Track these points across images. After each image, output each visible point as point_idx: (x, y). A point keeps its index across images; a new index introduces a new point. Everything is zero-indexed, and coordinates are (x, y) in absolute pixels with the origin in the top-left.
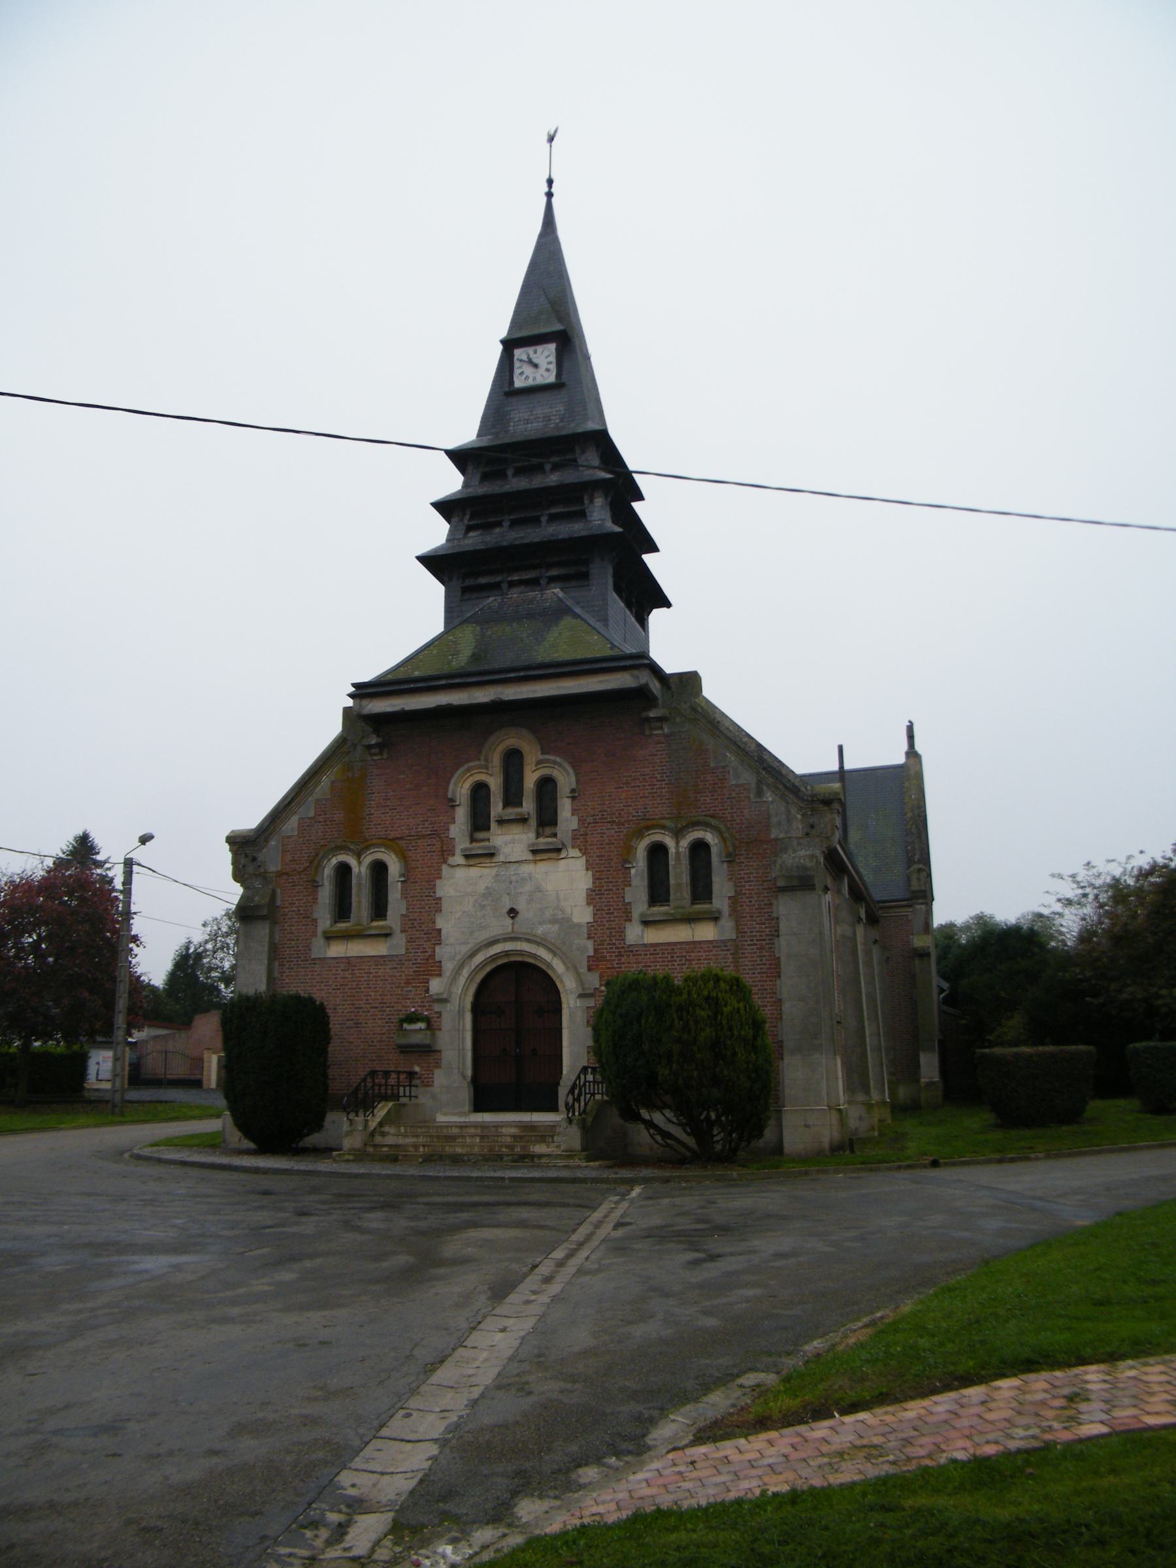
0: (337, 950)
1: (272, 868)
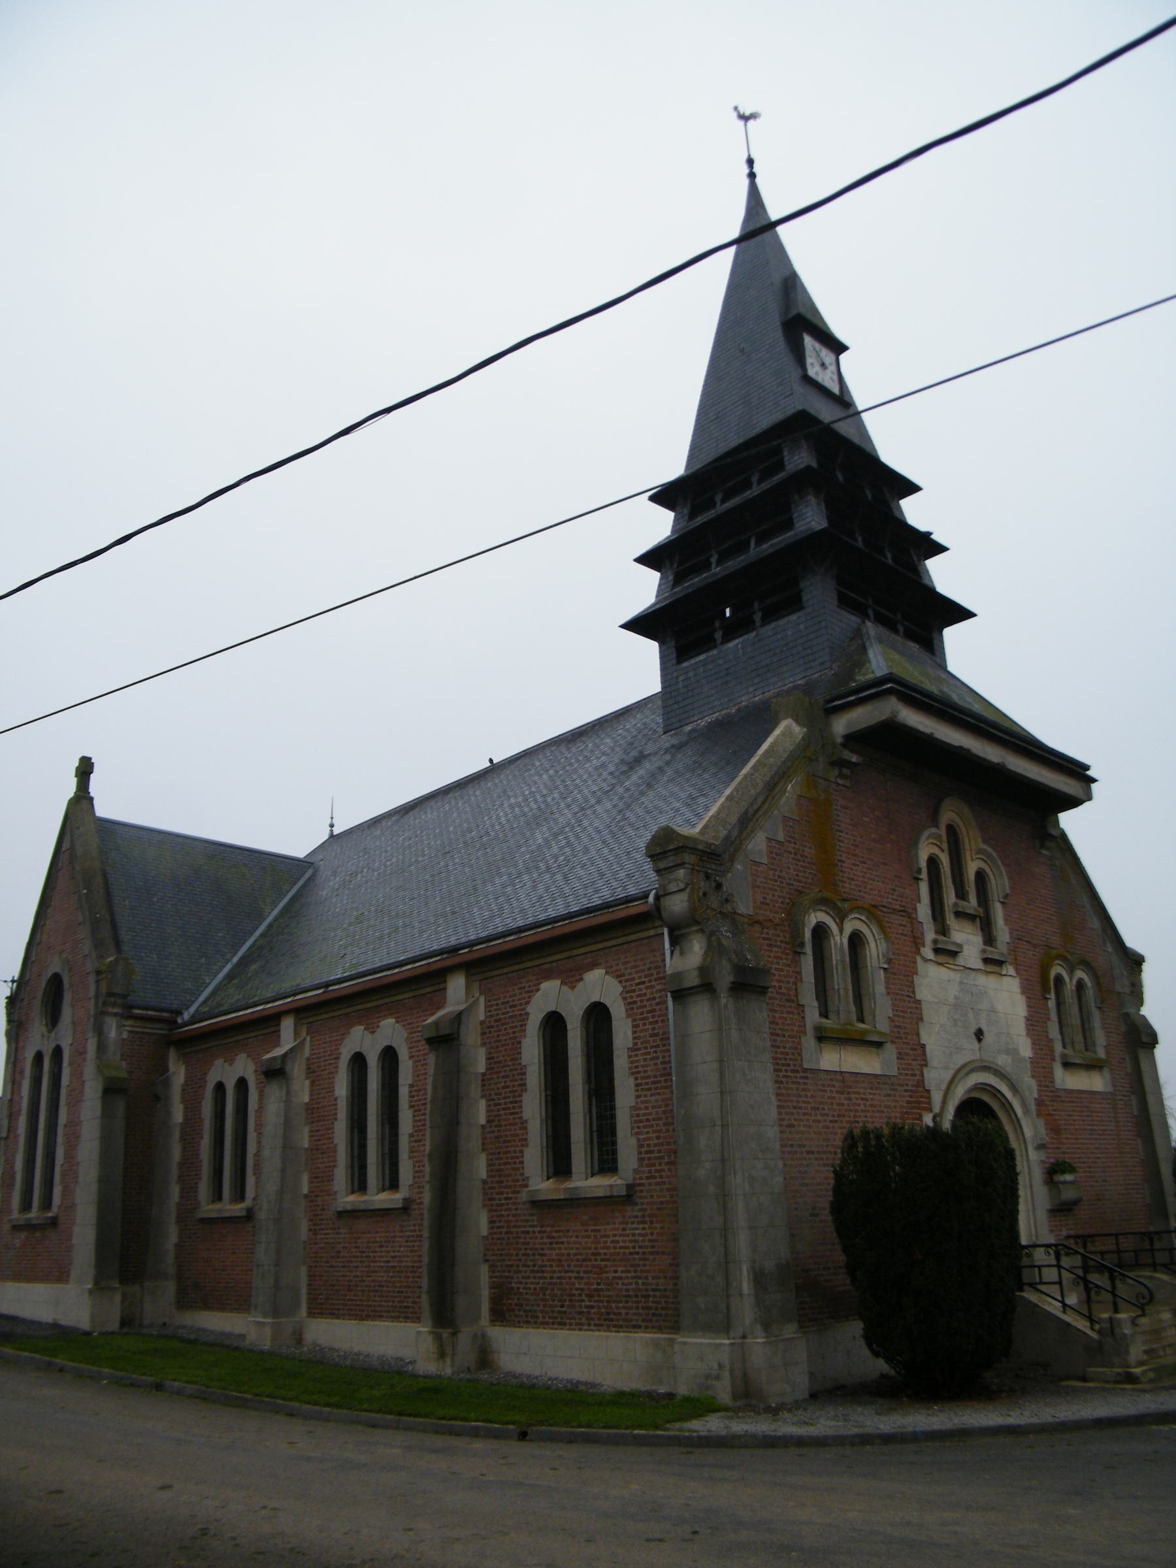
0: (831, 1059)
1: (742, 909)
